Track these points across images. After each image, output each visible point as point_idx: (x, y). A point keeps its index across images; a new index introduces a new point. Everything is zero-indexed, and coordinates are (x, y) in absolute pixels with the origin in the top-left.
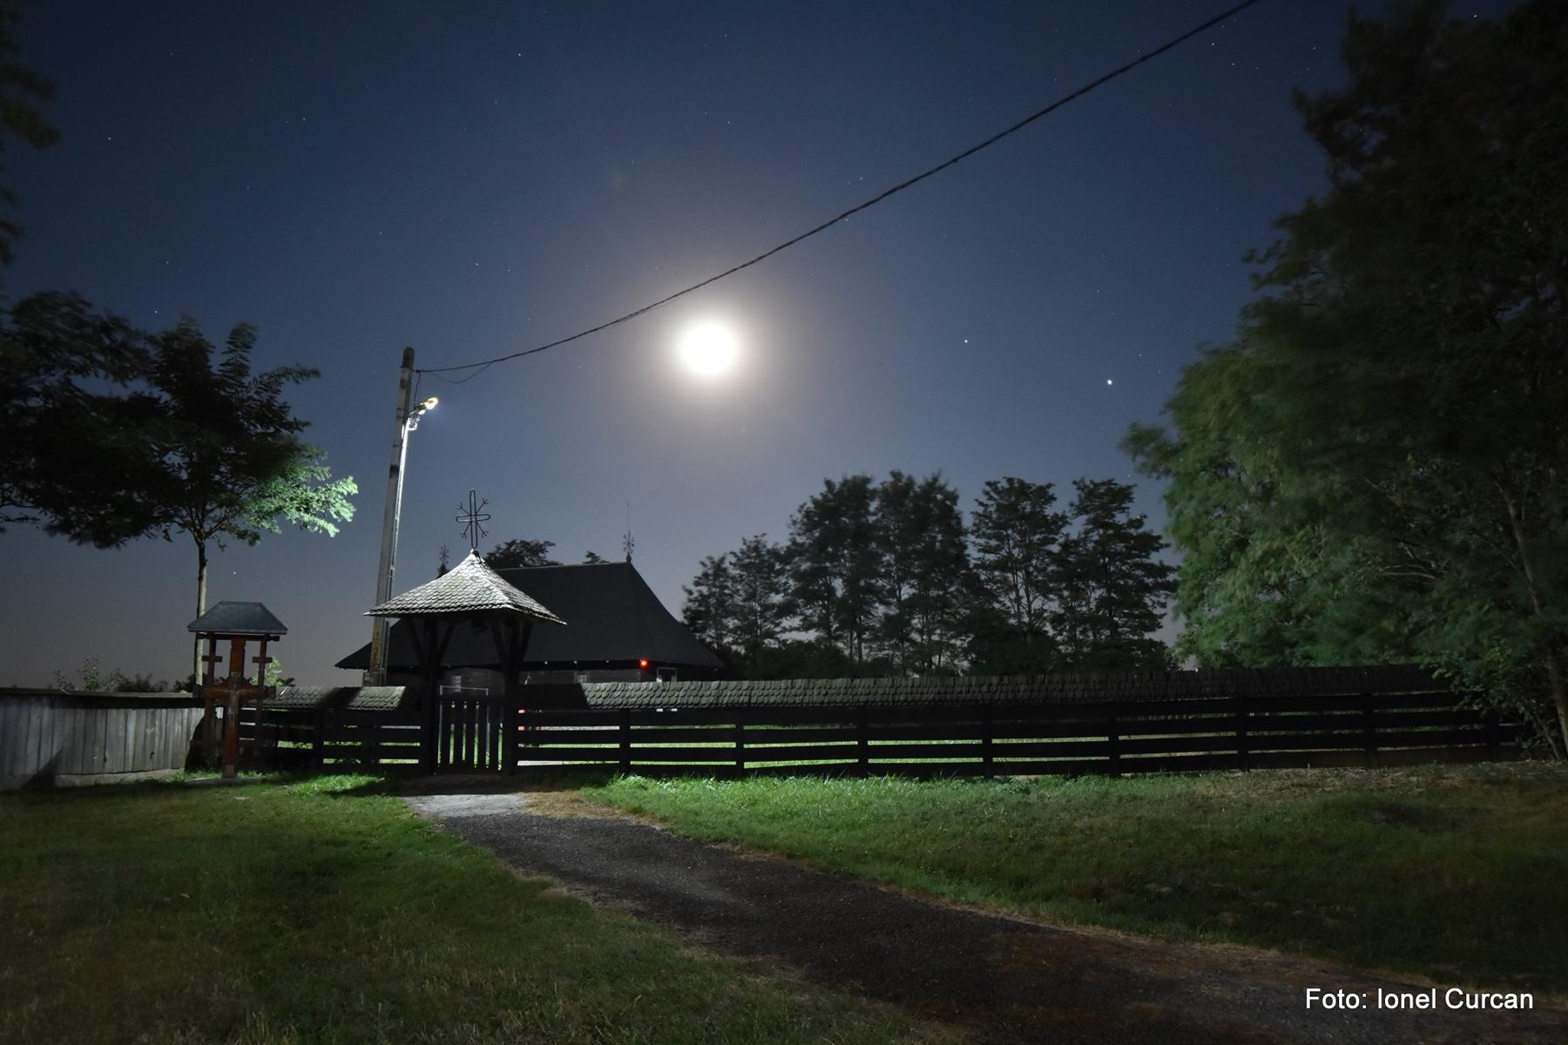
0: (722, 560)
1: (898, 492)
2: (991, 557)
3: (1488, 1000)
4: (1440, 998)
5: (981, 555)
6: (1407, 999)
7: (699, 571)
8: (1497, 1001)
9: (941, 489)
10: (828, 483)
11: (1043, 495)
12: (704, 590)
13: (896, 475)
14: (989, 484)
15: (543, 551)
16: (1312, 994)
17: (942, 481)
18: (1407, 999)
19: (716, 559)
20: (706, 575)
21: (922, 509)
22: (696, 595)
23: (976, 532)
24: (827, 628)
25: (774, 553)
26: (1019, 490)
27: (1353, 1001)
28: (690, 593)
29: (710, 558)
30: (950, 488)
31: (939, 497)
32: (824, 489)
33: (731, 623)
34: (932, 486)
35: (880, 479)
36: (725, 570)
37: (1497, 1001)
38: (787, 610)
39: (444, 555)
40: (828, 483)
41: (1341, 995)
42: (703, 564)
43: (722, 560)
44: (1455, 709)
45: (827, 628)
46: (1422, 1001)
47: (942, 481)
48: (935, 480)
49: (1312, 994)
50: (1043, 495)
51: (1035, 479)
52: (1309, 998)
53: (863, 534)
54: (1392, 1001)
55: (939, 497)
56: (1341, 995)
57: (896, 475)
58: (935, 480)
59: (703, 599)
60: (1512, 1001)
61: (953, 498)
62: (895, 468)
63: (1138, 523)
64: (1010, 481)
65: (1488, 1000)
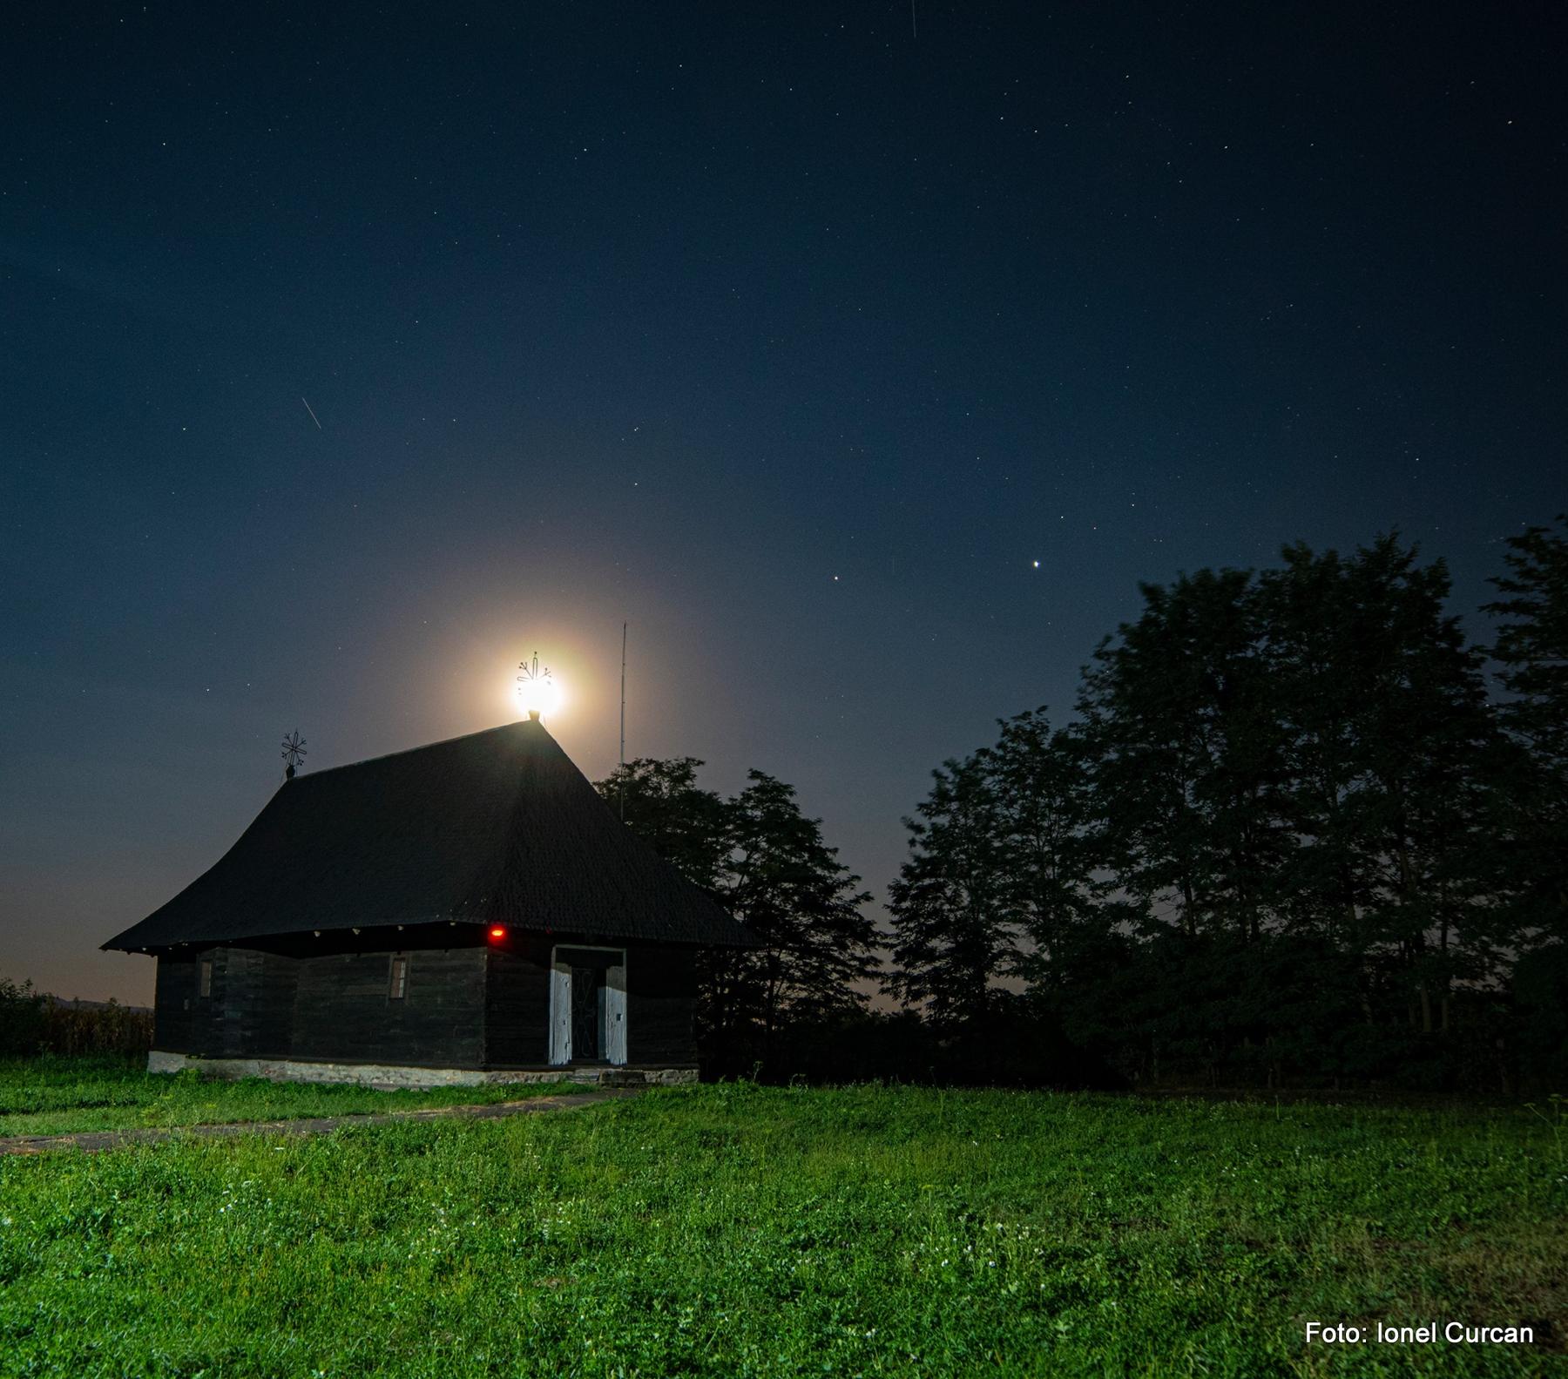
1: (1310, 593)
2: (1539, 699)
3: (1488, 1334)
4: (1440, 1332)
5: (1515, 697)
6: (1407, 1334)
7: (925, 789)
8: (1497, 1335)
10: (1151, 593)
12: (943, 820)
15: (688, 775)
16: (1313, 1328)
18: (1407, 1334)
20: (942, 796)
23: (1501, 653)
27: (1353, 1335)
28: (919, 829)
30: (1420, 564)
34: (1383, 558)
37: (1497, 1335)
40: (1151, 593)
41: (1341, 1329)
42: (936, 774)
44: (1478, 985)
46: (1421, 1335)
47: (1403, 546)
49: (1313, 1328)
52: (1309, 1332)
54: (1392, 1335)
56: (1341, 1329)
60: (1512, 1335)
61: (1437, 580)
62: (535, 709)
65: (1488, 1334)
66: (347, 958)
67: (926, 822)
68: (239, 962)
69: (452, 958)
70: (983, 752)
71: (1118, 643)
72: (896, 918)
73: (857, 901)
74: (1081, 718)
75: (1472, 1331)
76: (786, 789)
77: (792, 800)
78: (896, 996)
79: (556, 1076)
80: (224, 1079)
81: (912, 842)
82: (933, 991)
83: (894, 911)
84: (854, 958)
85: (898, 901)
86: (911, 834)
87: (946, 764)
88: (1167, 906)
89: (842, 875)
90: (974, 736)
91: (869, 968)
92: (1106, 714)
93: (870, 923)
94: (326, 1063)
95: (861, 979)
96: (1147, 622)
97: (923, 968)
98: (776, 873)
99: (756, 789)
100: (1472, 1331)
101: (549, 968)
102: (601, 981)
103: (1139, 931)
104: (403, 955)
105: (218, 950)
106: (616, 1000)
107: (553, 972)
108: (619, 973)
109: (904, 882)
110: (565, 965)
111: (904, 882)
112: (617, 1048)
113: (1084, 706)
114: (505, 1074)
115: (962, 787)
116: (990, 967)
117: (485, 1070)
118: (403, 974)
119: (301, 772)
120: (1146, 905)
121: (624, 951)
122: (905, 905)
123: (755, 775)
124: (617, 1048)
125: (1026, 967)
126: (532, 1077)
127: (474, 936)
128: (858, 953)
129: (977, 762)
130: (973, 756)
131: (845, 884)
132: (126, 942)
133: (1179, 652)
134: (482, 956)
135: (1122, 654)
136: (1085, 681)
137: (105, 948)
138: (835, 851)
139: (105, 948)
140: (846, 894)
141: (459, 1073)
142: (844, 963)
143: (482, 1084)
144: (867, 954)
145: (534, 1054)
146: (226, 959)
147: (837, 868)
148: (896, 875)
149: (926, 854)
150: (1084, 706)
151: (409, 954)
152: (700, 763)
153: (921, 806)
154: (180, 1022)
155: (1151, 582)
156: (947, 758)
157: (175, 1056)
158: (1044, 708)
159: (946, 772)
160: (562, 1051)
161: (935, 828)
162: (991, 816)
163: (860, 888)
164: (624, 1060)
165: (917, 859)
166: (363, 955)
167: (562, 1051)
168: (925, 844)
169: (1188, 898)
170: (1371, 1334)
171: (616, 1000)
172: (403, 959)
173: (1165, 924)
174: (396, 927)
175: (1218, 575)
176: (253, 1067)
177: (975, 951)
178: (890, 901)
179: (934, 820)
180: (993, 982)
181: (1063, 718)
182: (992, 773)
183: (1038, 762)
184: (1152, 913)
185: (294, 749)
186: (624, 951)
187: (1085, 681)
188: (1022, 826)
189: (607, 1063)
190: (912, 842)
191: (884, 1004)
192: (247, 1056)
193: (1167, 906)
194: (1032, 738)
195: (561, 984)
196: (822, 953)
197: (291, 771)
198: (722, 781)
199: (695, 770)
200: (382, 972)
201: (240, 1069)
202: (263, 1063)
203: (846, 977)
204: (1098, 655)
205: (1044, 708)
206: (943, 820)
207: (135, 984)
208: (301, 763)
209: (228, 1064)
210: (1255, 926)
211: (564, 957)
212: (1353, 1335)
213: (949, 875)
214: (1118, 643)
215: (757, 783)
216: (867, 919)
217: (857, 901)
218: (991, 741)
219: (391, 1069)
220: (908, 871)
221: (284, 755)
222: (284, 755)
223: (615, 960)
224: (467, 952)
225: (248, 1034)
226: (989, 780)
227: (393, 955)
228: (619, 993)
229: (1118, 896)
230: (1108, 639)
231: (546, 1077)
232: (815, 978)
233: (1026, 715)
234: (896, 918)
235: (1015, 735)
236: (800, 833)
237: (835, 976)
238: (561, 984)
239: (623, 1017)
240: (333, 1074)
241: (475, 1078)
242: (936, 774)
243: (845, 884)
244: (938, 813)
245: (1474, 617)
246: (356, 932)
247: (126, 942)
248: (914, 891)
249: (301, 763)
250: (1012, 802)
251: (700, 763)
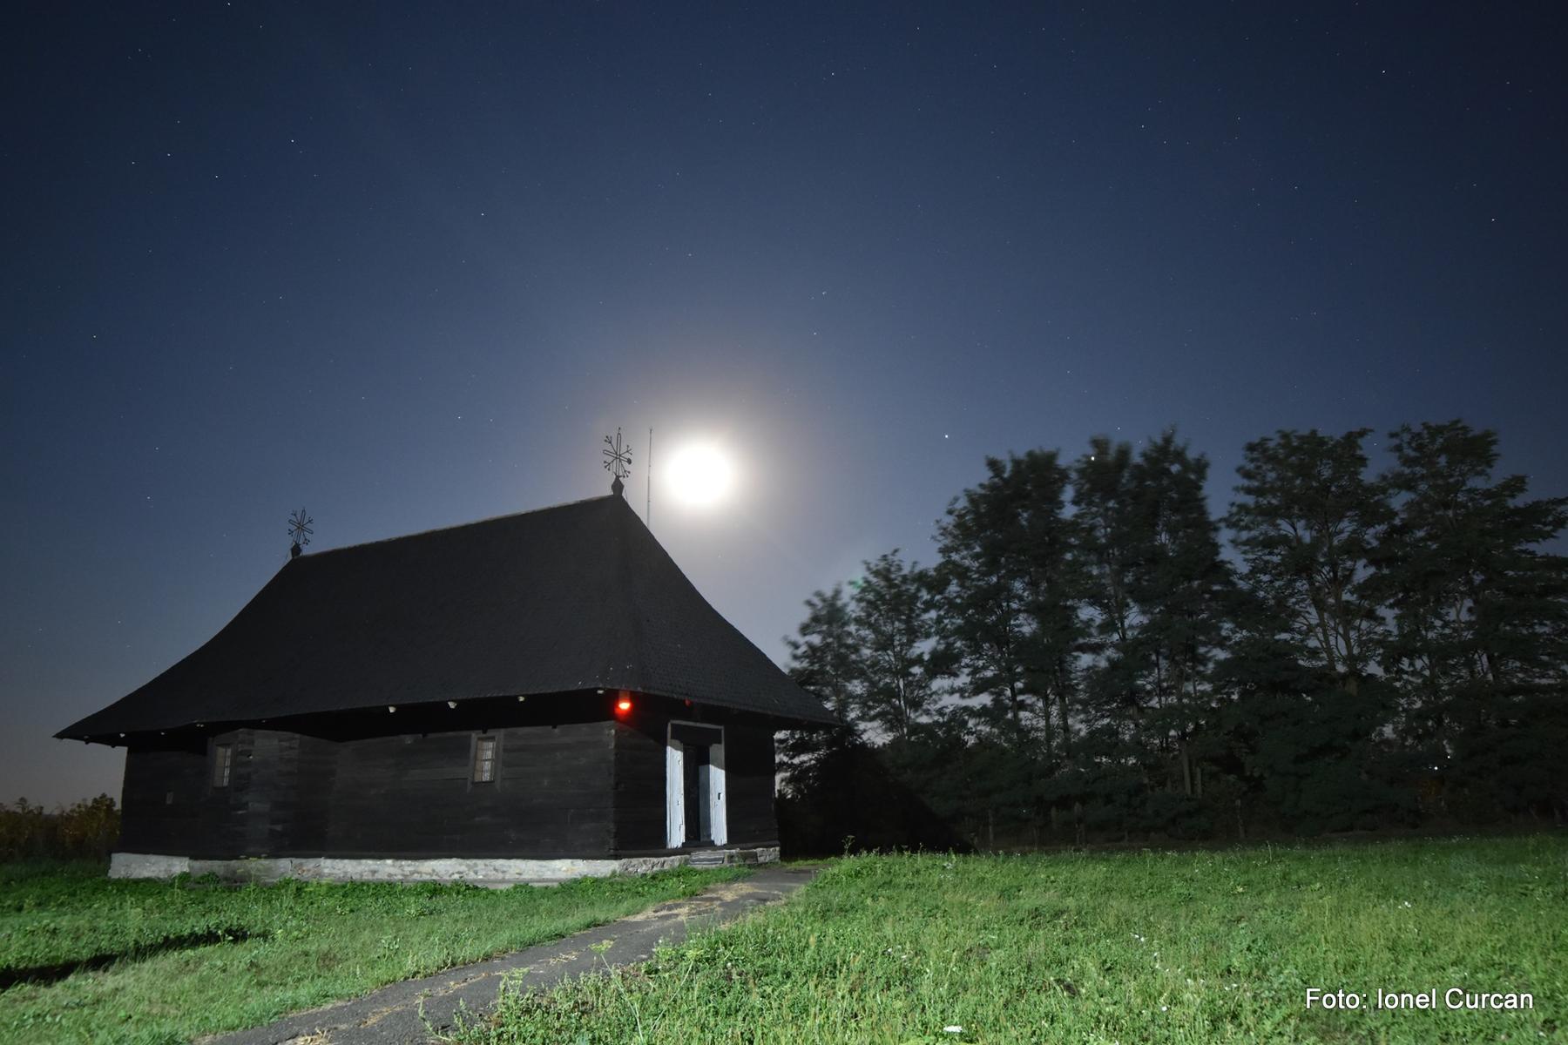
0: (837, 593)
1: (1104, 474)
3: (1488, 1000)
4: (1441, 996)
7: (805, 615)
9: (1179, 456)
10: (993, 465)
11: (1348, 452)
12: (816, 639)
13: (1100, 445)
14: (1251, 448)
17: (1178, 441)
19: (829, 593)
20: (816, 619)
21: (1150, 491)
22: (803, 649)
23: (1231, 523)
24: (1288, 456)
25: (921, 578)
26: (1313, 446)
27: (1353, 1001)
28: (796, 646)
29: (818, 594)
30: (1191, 455)
31: (1175, 468)
32: (986, 476)
33: (857, 687)
34: (1164, 452)
35: (1072, 453)
36: (841, 610)
38: (942, 664)
39: (301, 527)
40: (993, 465)
41: (1341, 995)
42: (809, 603)
43: (837, 593)
45: (1288, 456)
47: (1178, 441)
48: (1168, 440)
50: (1348, 452)
51: (1332, 430)
53: (1053, 536)
54: (1392, 1001)
55: (1175, 468)
57: (1100, 445)
58: (1168, 440)
59: (814, 653)
61: (1201, 467)
63: (1516, 485)
64: (1285, 436)
65: (1488, 1000)
66: (408, 740)
67: (801, 640)
68: (268, 746)
69: (582, 731)
75: (1526, 1004)
80: (234, 883)
94: (381, 858)
100: (1526, 1004)
102: (706, 761)
104: (491, 733)
105: (242, 732)
107: (669, 749)
108: (718, 751)
110: (677, 742)
112: (719, 830)
114: (635, 861)
117: (616, 857)
118: (489, 754)
119: (307, 551)
124: (719, 830)
127: (601, 708)
132: (92, 730)
133: (1010, 516)
134: (609, 731)
137: (61, 735)
139: (61, 735)
141: (579, 862)
143: (614, 872)
145: (650, 838)
146: (252, 743)
151: (500, 734)
154: (143, 821)
156: (815, 589)
157: (153, 858)
159: (816, 601)
160: (677, 835)
164: (725, 841)
166: (431, 736)
167: (677, 835)
171: (717, 778)
172: (492, 739)
174: (516, 698)
176: (285, 867)
179: (808, 638)
192: (276, 854)
195: (675, 760)
197: (296, 550)
200: (463, 753)
201: (268, 870)
202: (296, 861)
204: (950, 512)
207: (104, 772)
208: (307, 542)
209: (255, 865)
212: (1353, 1001)
219: (479, 862)
221: (291, 532)
224: (584, 728)
225: (279, 828)
227: (474, 735)
230: (956, 499)
235: (877, 573)
238: (675, 760)
239: (723, 796)
240: (392, 870)
241: (604, 868)
245: (1221, 495)
246: (452, 705)
247: (92, 730)
249: (307, 542)
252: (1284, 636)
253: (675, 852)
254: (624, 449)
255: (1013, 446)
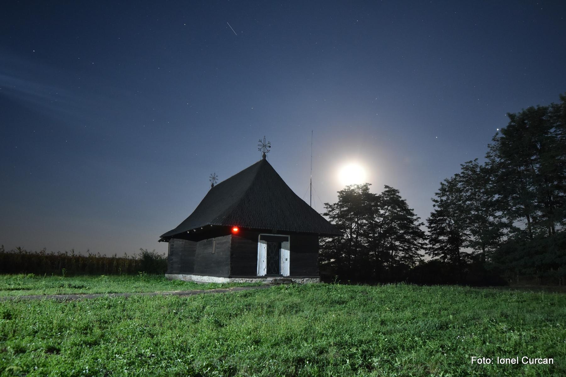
3: (537, 361)
7: (437, 188)
8: (540, 361)
10: (512, 117)
12: (444, 198)
16: (474, 358)
20: (443, 190)
27: (488, 361)
28: (436, 201)
37: (540, 361)
39: (214, 178)
40: (512, 117)
41: (484, 359)
49: (474, 358)
52: (472, 360)
54: (502, 361)
56: (484, 359)
65: (537, 361)
67: (439, 199)
70: (456, 175)
71: (501, 135)
72: (430, 230)
73: (419, 225)
74: (487, 160)
75: (532, 360)
76: (396, 191)
77: (399, 194)
78: (430, 255)
79: (258, 280)
81: (434, 206)
82: (443, 253)
83: (429, 228)
84: (420, 243)
85: (430, 225)
86: (434, 203)
87: (445, 180)
88: (521, 224)
89: (415, 217)
90: (452, 170)
91: (425, 246)
92: (498, 160)
93: (424, 232)
95: (422, 250)
96: (509, 126)
97: (437, 246)
98: (395, 217)
99: (386, 191)
100: (532, 360)
101: (257, 242)
103: (510, 232)
106: (285, 254)
107: (259, 243)
108: (288, 244)
109: (431, 218)
111: (431, 218)
112: (286, 269)
113: (488, 157)
114: (237, 279)
115: (450, 188)
116: (460, 245)
117: (229, 277)
120: (511, 223)
121: (289, 236)
122: (432, 225)
123: (386, 187)
124: (286, 269)
125: (473, 244)
126: (249, 280)
127: (226, 231)
128: (420, 242)
129: (455, 179)
130: (454, 177)
131: (416, 220)
135: (502, 138)
136: (490, 149)
138: (413, 210)
140: (416, 223)
142: (415, 245)
144: (423, 242)
145: (251, 271)
147: (414, 215)
148: (429, 216)
149: (439, 209)
150: (488, 157)
152: (370, 184)
153: (437, 194)
155: (511, 113)
158: (476, 159)
160: (262, 269)
161: (442, 201)
162: (461, 196)
163: (420, 221)
164: (289, 275)
165: (436, 211)
167: (262, 269)
168: (439, 206)
169: (529, 220)
170: (494, 361)
171: (285, 254)
173: (519, 229)
175: (536, 108)
177: (456, 241)
178: (427, 224)
180: (462, 250)
181: (482, 162)
182: (460, 182)
183: (475, 177)
184: (514, 225)
185: (214, 178)
186: (289, 236)
187: (490, 149)
188: (470, 199)
189: (282, 276)
190: (434, 206)
191: (427, 258)
193: (521, 224)
194: (473, 170)
195: (262, 249)
196: (408, 241)
198: (376, 190)
199: (369, 187)
203: (417, 249)
205: (476, 159)
206: (444, 198)
210: (553, 229)
211: (264, 239)
212: (488, 361)
213: (448, 217)
214: (501, 135)
215: (387, 189)
216: (423, 231)
217: (419, 225)
218: (459, 171)
220: (433, 215)
222: (210, 180)
223: (286, 240)
226: (460, 184)
228: (287, 251)
229: (504, 220)
231: (254, 281)
232: (406, 251)
233: (471, 162)
234: (430, 230)
235: (467, 168)
236: (402, 204)
237: (414, 249)
238: (262, 249)
239: (289, 260)
242: (441, 184)
243: (416, 220)
244: (443, 196)
248: (434, 220)
250: (467, 191)
251: (370, 184)
252: (504, 170)
253: (262, 277)
254: (267, 143)
255: (519, 109)
